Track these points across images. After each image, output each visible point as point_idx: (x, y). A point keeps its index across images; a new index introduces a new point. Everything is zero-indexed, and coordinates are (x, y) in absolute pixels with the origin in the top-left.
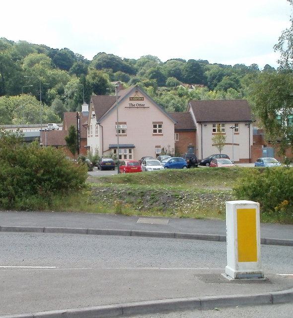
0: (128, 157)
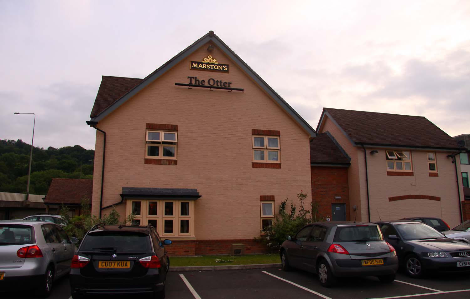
0: (177, 226)
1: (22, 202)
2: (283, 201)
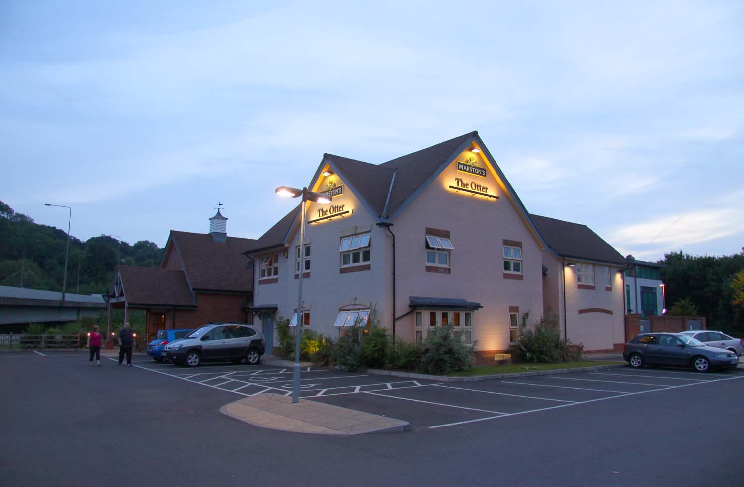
1: (59, 301)
2: (525, 313)
